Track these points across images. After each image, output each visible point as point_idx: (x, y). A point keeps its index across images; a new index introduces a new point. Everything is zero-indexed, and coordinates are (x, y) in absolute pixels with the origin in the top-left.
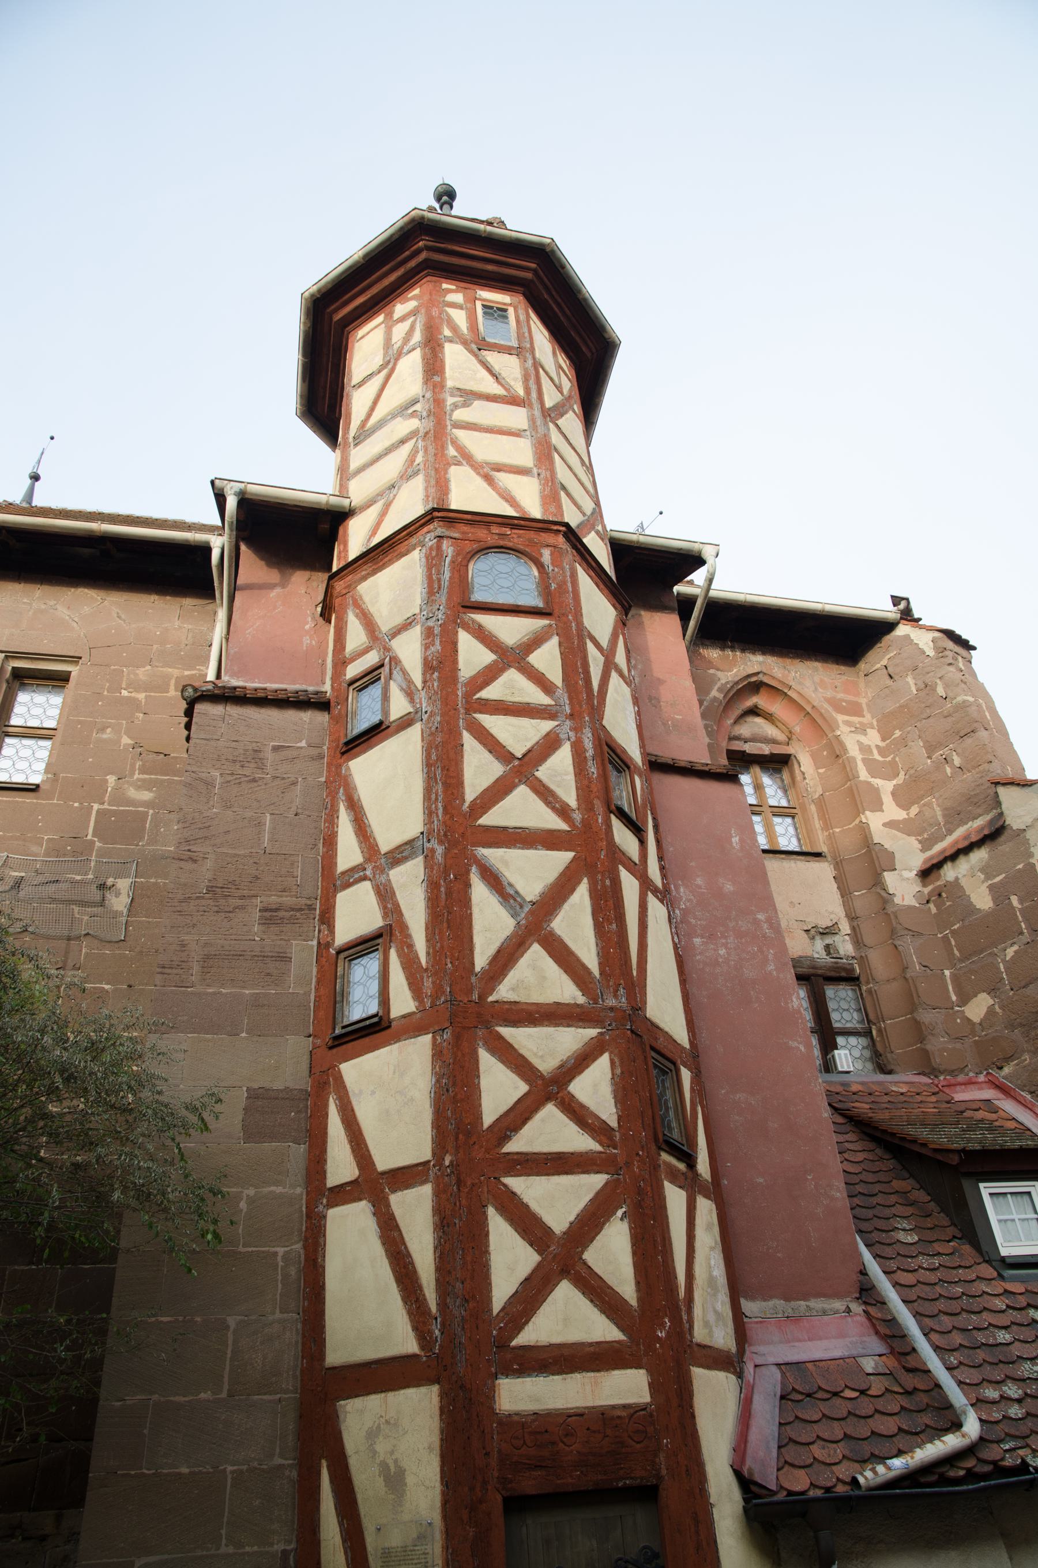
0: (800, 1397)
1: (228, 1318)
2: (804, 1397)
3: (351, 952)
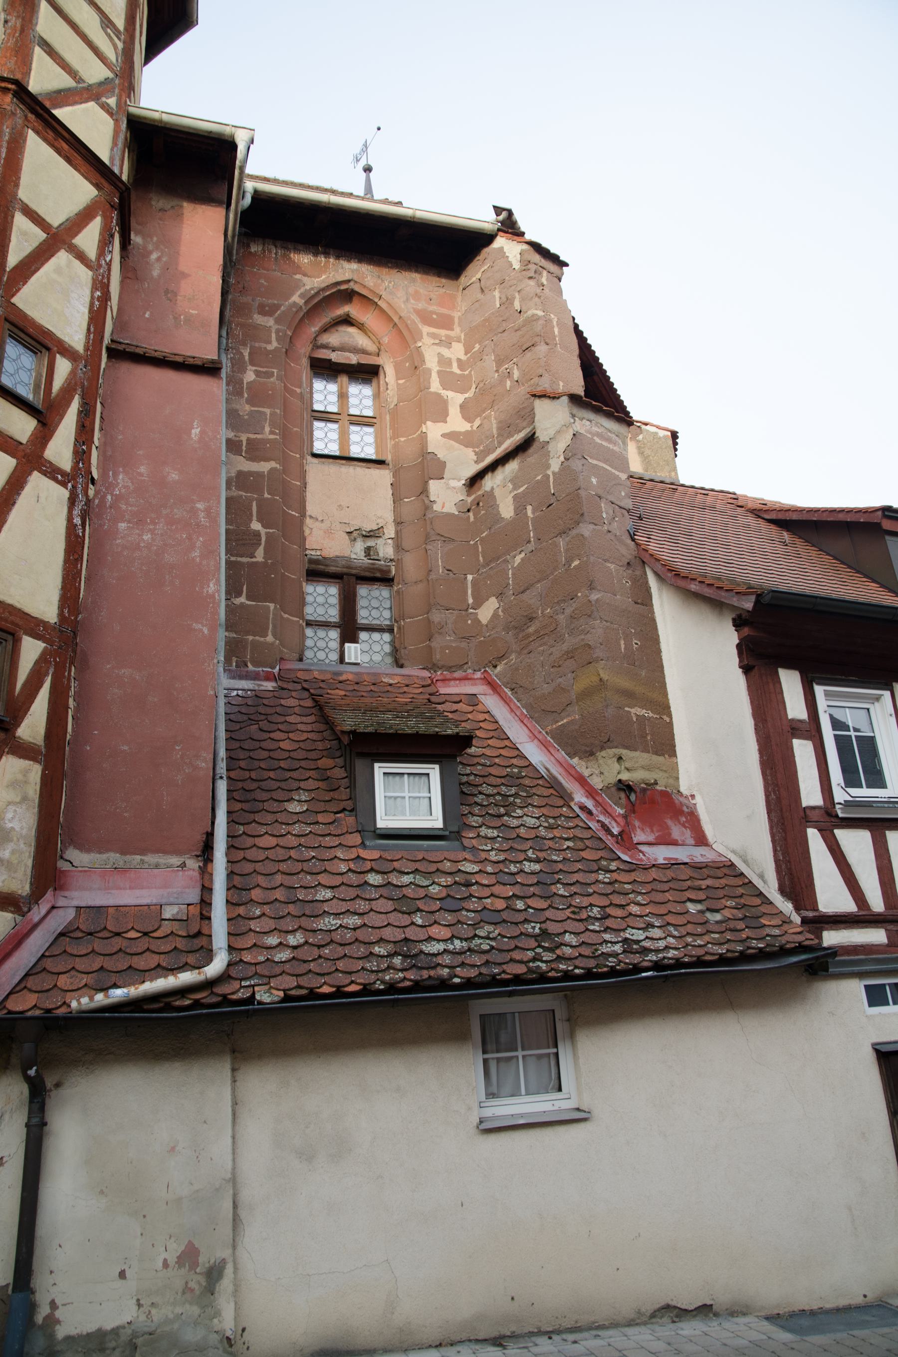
0: (80, 935)
2: (84, 934)
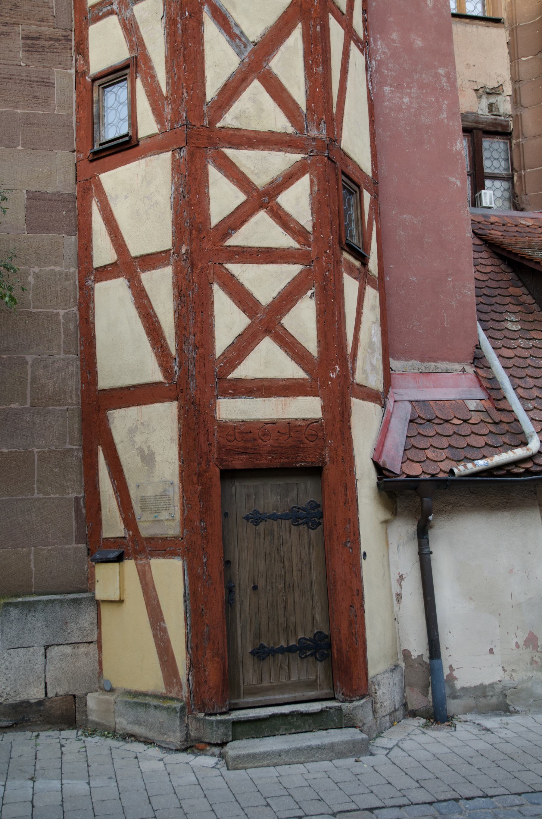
0: (423, 422)
1: (26, 357)
2: (425, 421)
3: (104, 80)
